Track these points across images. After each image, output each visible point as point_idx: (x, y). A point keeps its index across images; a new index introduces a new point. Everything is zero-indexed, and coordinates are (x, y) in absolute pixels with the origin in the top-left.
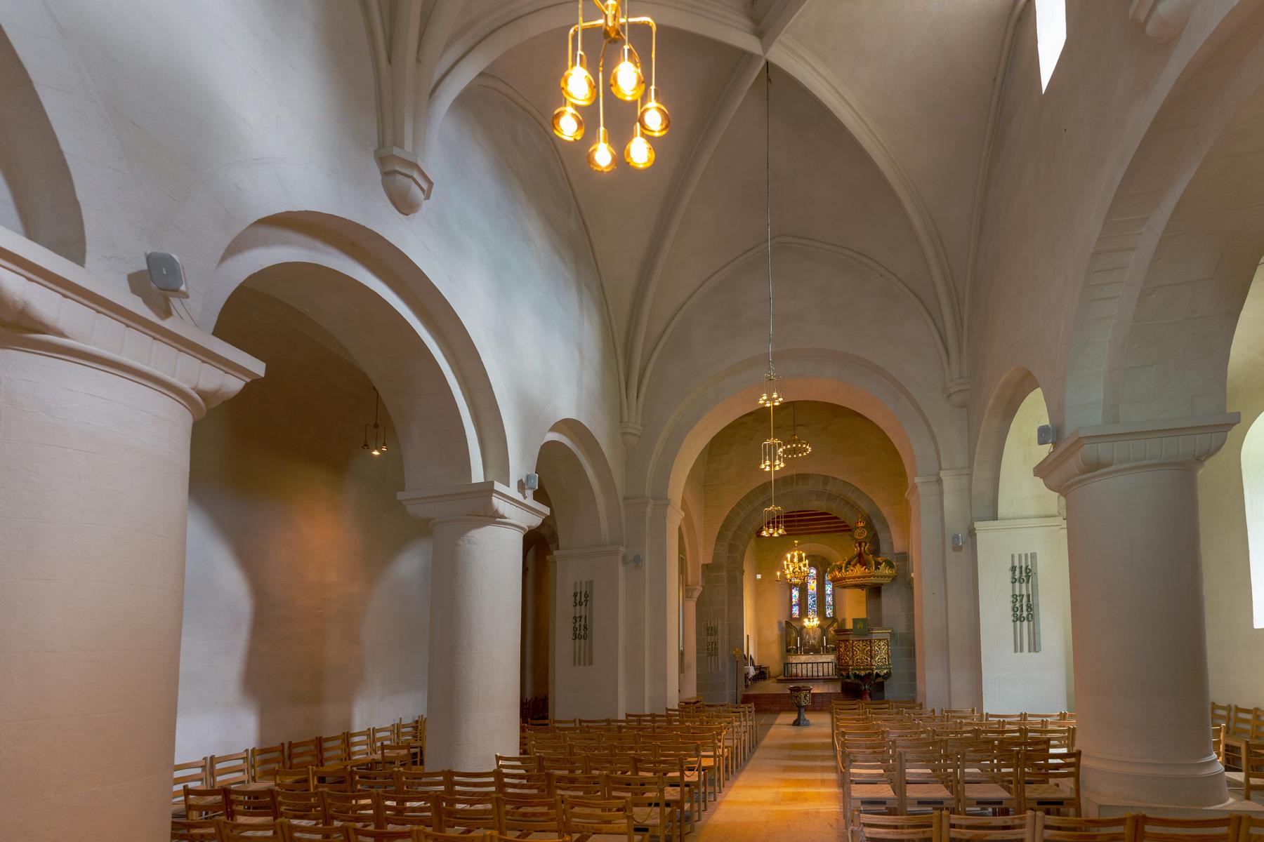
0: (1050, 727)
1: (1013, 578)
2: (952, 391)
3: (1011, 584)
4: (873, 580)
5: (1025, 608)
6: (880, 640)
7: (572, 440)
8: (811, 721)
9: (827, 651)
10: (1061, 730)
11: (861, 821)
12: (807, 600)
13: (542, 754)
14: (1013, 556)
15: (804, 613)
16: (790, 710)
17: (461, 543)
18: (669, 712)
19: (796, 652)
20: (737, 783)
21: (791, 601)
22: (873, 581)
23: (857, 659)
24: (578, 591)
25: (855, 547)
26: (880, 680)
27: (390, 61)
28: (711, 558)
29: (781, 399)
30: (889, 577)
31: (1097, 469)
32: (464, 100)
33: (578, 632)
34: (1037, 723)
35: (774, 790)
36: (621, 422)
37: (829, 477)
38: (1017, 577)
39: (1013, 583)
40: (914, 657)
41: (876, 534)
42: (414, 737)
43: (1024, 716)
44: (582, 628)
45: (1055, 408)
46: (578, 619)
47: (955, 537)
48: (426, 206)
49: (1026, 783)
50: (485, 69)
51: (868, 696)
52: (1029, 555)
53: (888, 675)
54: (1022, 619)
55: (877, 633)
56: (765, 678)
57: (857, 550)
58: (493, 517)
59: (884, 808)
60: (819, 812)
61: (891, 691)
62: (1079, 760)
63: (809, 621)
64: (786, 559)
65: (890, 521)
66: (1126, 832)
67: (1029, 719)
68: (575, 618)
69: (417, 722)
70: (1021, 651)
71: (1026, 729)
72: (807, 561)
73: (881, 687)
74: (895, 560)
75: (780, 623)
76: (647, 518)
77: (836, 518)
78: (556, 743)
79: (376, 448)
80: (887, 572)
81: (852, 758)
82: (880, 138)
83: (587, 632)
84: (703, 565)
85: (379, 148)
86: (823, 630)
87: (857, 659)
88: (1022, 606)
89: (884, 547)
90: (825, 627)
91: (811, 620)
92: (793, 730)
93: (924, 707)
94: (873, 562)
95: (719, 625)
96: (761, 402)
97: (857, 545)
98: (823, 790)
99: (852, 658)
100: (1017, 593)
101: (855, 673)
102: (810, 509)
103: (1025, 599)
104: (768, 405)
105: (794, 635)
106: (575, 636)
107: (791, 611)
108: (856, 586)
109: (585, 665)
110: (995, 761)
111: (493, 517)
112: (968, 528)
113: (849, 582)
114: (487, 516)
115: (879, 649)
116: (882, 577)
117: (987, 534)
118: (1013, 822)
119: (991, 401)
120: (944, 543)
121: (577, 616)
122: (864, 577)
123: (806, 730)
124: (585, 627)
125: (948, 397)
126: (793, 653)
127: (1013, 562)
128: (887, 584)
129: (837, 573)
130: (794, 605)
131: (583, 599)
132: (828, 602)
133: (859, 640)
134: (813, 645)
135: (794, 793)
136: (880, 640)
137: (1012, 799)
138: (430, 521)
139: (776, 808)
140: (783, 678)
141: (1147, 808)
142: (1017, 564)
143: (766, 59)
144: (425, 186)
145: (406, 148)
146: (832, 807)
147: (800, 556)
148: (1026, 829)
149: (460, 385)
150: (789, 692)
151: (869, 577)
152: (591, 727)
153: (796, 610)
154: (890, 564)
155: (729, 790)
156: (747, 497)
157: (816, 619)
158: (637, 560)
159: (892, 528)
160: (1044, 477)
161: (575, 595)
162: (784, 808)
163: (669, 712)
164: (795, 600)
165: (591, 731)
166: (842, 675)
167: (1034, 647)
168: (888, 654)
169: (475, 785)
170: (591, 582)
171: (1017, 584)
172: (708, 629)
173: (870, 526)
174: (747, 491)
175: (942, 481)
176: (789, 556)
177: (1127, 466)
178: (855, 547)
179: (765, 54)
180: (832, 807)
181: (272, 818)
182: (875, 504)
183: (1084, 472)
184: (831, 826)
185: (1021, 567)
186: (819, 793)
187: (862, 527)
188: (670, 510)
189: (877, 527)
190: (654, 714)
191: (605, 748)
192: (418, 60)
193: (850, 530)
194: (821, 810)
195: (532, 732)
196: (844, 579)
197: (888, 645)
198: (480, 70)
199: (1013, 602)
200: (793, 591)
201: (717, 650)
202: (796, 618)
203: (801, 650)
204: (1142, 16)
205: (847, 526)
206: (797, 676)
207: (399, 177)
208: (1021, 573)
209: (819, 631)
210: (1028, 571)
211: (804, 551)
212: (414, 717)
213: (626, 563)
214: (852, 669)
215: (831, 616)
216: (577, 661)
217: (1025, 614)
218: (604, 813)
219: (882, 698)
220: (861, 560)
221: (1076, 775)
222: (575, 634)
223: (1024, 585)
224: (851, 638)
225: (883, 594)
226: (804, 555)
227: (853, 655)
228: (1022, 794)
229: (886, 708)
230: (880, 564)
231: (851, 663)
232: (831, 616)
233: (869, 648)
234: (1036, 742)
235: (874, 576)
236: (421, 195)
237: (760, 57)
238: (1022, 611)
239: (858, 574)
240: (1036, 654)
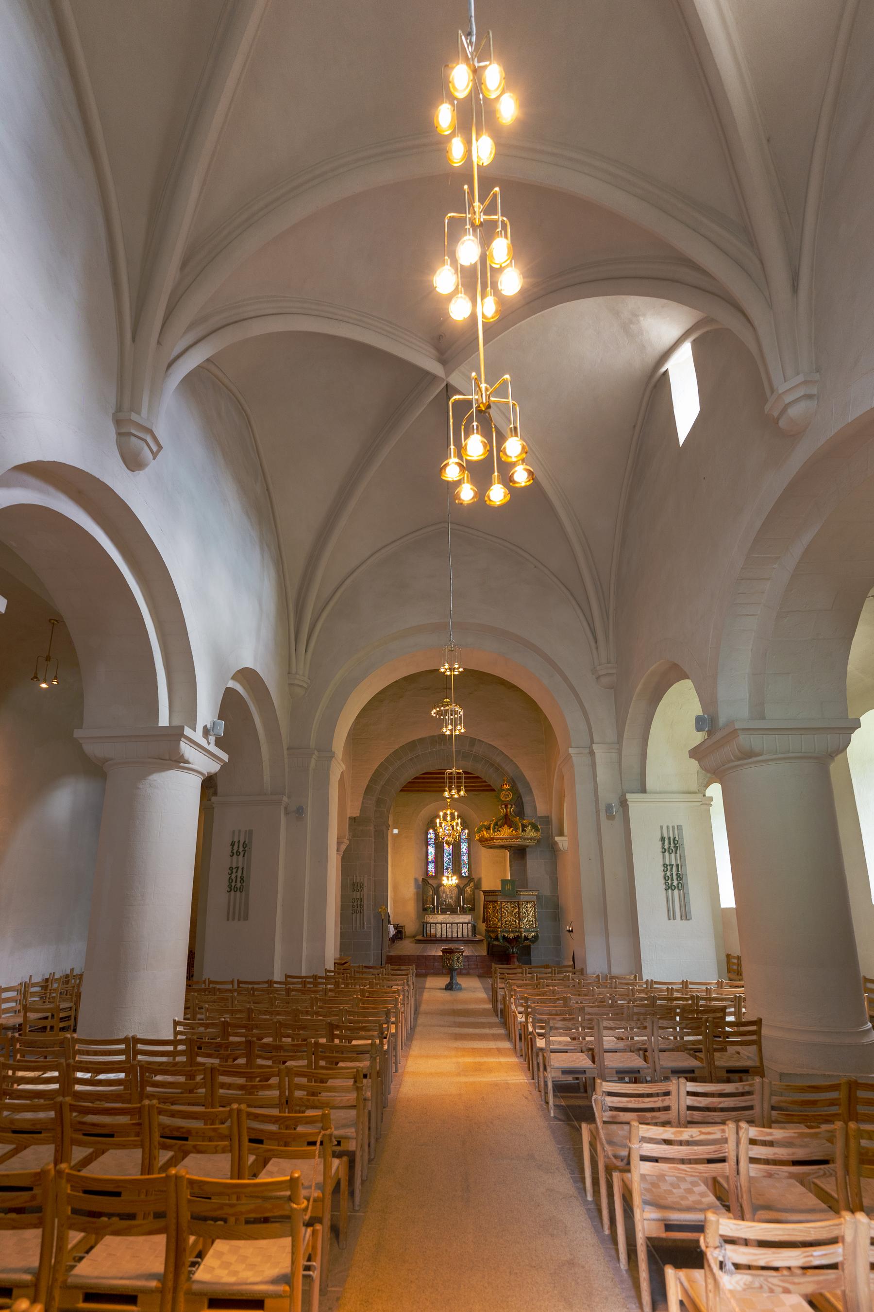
0: (676, 994)
1: (663, 848)
2: (601, 673)
3: (661, 854)
4: (520, 842)
5: (675, 877)
6: (527, 902)
7: (244, 688)
8: (464, 985)
9: (465, 911)
10: (685, 998)
11: (604, 1090)
12: (442, 857)
13: (228, 1020)
14: (661, 827)
15: (440, 871)
16: (437, 973)
17: (141, 786)
18: (328, 974)
19: (433, 912)
20: (412, 1053)
21: (427, 858)
23: (506, 921)
24: (236, 840)
25: (502, 808)
26: (527, 943)
27: (134, 340)
28: (359, 811)
29: (461, 670)
30: (535, 840)
31: (750, 757)
32: (191, 381)
33: (233, 884)
34: (702, 991)
35: (454, 1060)
36: (289, 673)
37: (476, 739)
38: (666, 847)
39: (663, 852)
40: (559, 921)
42: (41, 998)
43: (685, 984)
44: (239, 879)
45: (708, 699)
46: (234, 871)
47: (609, 807)
48: (153, 465)
49: (605, 1052)
50: (211, 357)
51: (516, 960)
52: (676, 827)
53: (536, 938)
54: (673, 888)
55: (524, 895)
56: (401, 938)
57: (503, 811)
58: (177, 761)
59: (571, 1079)
60: (508, 1084)
61: (539, 954)
62: (760, 1028)
63: (448, 880)
64: (439, 817)
66: (841, 1097)
67: (690, 986)
68: (231, 868)
69: (47, 980)
70: (674, 919)
71: (697, 996)
72: (459, 820)
73: (526, 951)
75: (416, 880)
76: (310, 769)
77: (478, 777)
78: (222, 1007)
79: (45, 681)
80: (533, 834)
81: (552, 1025)
82: (539, 456)
83: (244, 884)
84: (349, 818)
85: (116, 412)
86: (460, 889)
87: (506, 921)
88: (672, 875)
89: (528, 810)
90: (462, 886)
91: (450, 879)
92: (447, 995)
93: (584, 972)
94: (520, 825)
95: (366, 879)
96: (442, 670)
97: (503, 806)
98: (503, 1060)
99: (501, 920)
100: (668, 863)
101: (504, 936)
103: (674, 869)
104: (448, 673)
105: (431, 893)
106: (231, 888)
107: (428, 868)
108: (502, 847)
109: (239, 920)
110: (678, 1029)
111: (177, 761)
112: (620, 798)
113: (497, 843)
114: (171, 760)
117: (636, 804)
118: (743, 1089)
119: (639, 687)
120: (598, 811)
121: (234, 867)
122: (512, 839)
123: (461, 995)
124: (242, 879)
125: (598, 678)
126: (430, 913)
127: (662, 833)
128: (532, 846)
129: (485, 833)
130: (430, 862)
131: (241, 849)
132: (464, 860)
133: (508, 902)
134: (450, 905)
135: (475, 1063)
136: (527, 902)
137: (703, 1068)
138: (107, 761)
139: (463, 1079)
140: (423, 938)
141: (822, 1075)
142: (665, 835)
143: (447, 381)
144: (155, 449)
145: (142, 415)
146: (520, 1078)
147: (452, 815)
148: (754, 1096)
149: (155, 628)
150: (441, 954)
151: (517, 839)
152: (257, 990)
153: (431, 867)
154: (535, 828)
155: (407, 1060)
157: (455, 878)
158: (300, 811)
159: (535, 792)
160: (699, 760)
161: (233, 844)
162: (472, 1079)
163: (328, 974)
164: (431, 857)
165: (256, 993)
166: (491, 937)
167: (686, 915)
168: (535, 917)
169: (96, 1053)
170: (251, 832)
171: (667, 854)
172: (353, 885)
173: (514, 789)
174: (397, 747)
175: (594, 753)
176: (441, 814)
177: (774, 756)
178: (502, 808)
179: (447, 378)
180: (520, 1078)
182: (518, 767)
183: (739, 759)
184: (527, 1098)
185: (669, 838)
186: (500, 1063)
187: (507, 789)
188: (334, 761)
189: (522, 790)
190: (316, 976)
191: (240, 1011)
192: (159, 343)
193: (493, 790)
194: (510, 1082)
195: (196, 994)
196: (492, 839)
197: (534, 907)
198: (208, 357)
199: (664, 871)
200: (429, 847)
201: (363, 906)
202: (432, 876)
203: (438, 909)
204: (776, 414)
205: (490, 786)
206: (436, 936)
207: (133, 439)
208: (670, 844)
209: (456, 891)
210: (676, 842)
211: (456, 810)
212: (43, 975)
213: (288, 814)
215: (467, 875)
216: (230, 915)
217: (675, 883)
218: (309, 1084)
219: (529, 962)
220: (507, 821)
221: (758, 1043)
222: (230, 886)
223: (673, 855)
224: (500, 899)
225: (528, 857)
226: (456, 814)
227: (502, 916)
228: (712, 1062)
229: (519, 973)
230: (527, 827)
231: (499, 925)
232: (467, 875)
233: (517, 910)
234: (715, 1010)
236: (150, 456)
237: (443, 380)
238: (672, 880)
239: (506, 835)
240: (688, 922)
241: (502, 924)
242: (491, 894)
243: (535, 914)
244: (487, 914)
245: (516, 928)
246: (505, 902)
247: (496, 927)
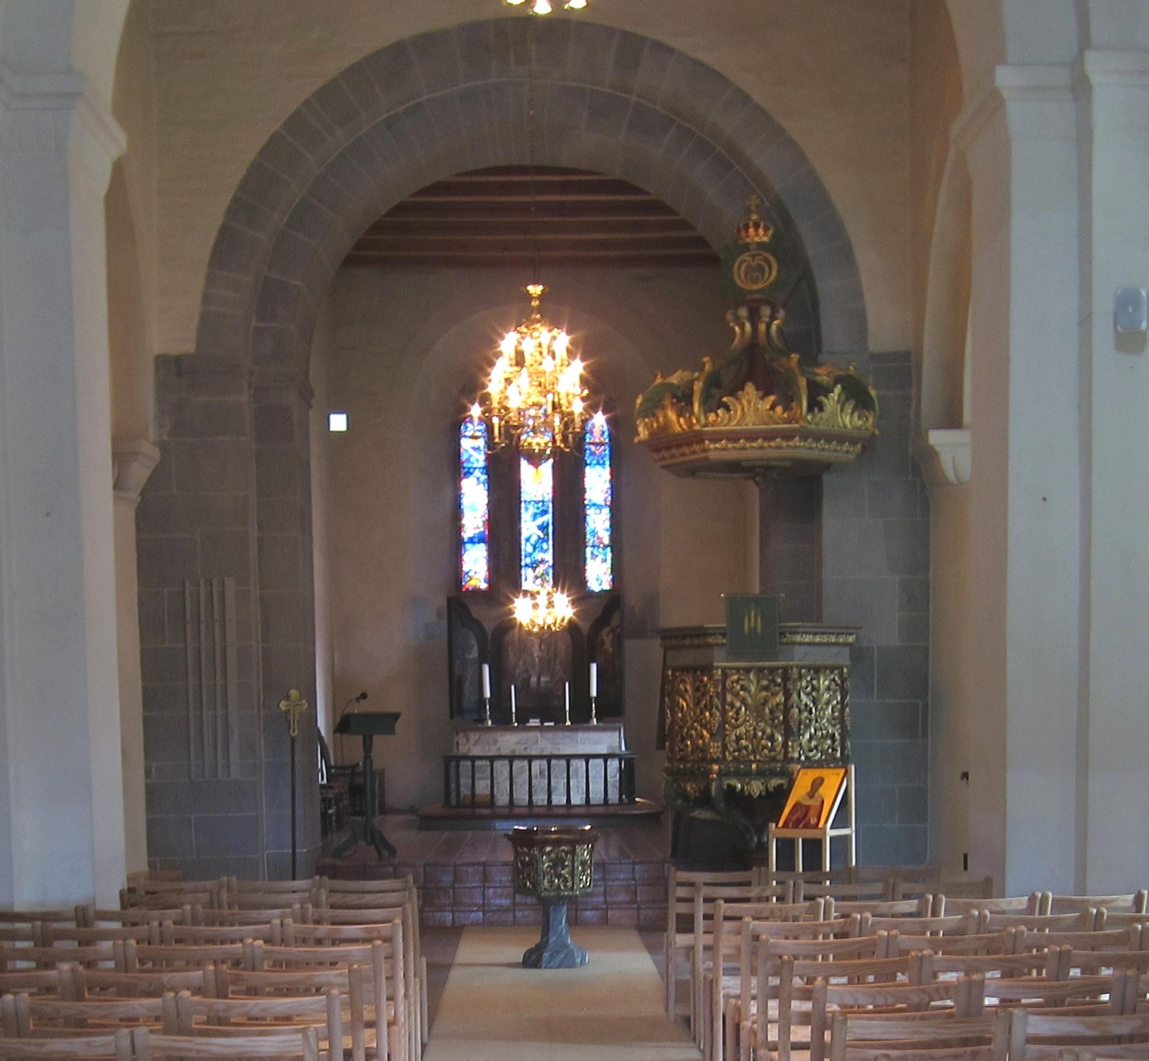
4: (800, 449)
22: (799, 454)
23: (738, 738)
30: (853, 441)
37: (642, 39)
40: (925, 735)
41: (807, 277)
65: (858, 230)
74: (871, 379)
80: (848, 420)
87: (738, 738)
89: (834, 330)
94: (803, 382)
97: (743, 312)
99: (719, 734)
101: (731, 788)
102: (564, 162)
113: (716, 451)
115: (815, 701)
116: (829, 438)
129: (672, 415)
130: (471, 540)
132: (594, 533)
133: (748, 670)
154: (857, 395)
156: (326, 95)
159: (865, 258)
168: (842, 720)
174: (332, 68)
181: (538, 720)
187: (761, 245)
189: (814, 248)
196: (698, 438)
214: (719, 773)
227: (724, 721)
230: (827, 391)
231: (714, 749)
233: (780, 698)
235: (805, 436)
239: (750, 425)
241: (725, 748)
242: (688, 642)
243: (842, 711)
244: (674, 714)
245: (774, 759)
246: (738, 670)
247: (704, 759)
